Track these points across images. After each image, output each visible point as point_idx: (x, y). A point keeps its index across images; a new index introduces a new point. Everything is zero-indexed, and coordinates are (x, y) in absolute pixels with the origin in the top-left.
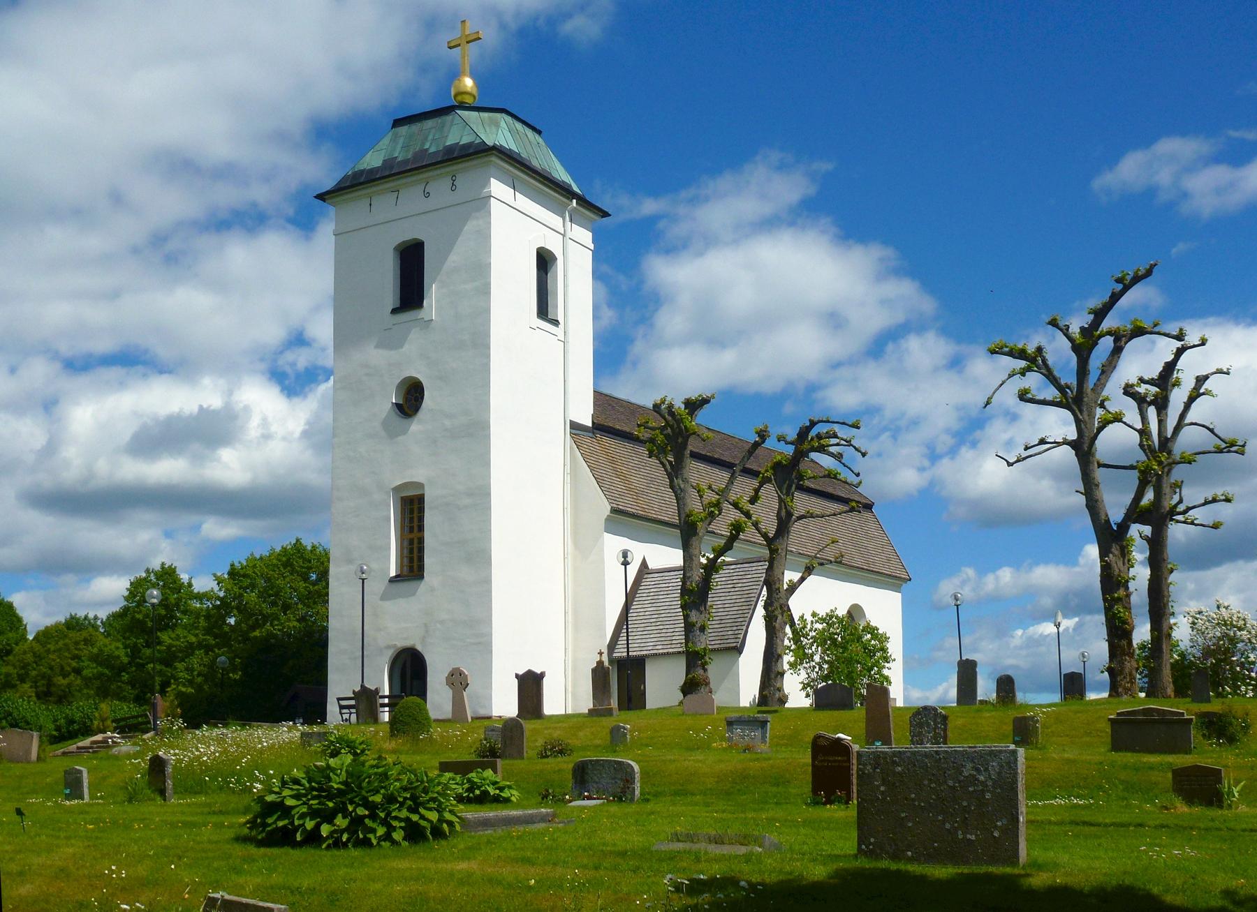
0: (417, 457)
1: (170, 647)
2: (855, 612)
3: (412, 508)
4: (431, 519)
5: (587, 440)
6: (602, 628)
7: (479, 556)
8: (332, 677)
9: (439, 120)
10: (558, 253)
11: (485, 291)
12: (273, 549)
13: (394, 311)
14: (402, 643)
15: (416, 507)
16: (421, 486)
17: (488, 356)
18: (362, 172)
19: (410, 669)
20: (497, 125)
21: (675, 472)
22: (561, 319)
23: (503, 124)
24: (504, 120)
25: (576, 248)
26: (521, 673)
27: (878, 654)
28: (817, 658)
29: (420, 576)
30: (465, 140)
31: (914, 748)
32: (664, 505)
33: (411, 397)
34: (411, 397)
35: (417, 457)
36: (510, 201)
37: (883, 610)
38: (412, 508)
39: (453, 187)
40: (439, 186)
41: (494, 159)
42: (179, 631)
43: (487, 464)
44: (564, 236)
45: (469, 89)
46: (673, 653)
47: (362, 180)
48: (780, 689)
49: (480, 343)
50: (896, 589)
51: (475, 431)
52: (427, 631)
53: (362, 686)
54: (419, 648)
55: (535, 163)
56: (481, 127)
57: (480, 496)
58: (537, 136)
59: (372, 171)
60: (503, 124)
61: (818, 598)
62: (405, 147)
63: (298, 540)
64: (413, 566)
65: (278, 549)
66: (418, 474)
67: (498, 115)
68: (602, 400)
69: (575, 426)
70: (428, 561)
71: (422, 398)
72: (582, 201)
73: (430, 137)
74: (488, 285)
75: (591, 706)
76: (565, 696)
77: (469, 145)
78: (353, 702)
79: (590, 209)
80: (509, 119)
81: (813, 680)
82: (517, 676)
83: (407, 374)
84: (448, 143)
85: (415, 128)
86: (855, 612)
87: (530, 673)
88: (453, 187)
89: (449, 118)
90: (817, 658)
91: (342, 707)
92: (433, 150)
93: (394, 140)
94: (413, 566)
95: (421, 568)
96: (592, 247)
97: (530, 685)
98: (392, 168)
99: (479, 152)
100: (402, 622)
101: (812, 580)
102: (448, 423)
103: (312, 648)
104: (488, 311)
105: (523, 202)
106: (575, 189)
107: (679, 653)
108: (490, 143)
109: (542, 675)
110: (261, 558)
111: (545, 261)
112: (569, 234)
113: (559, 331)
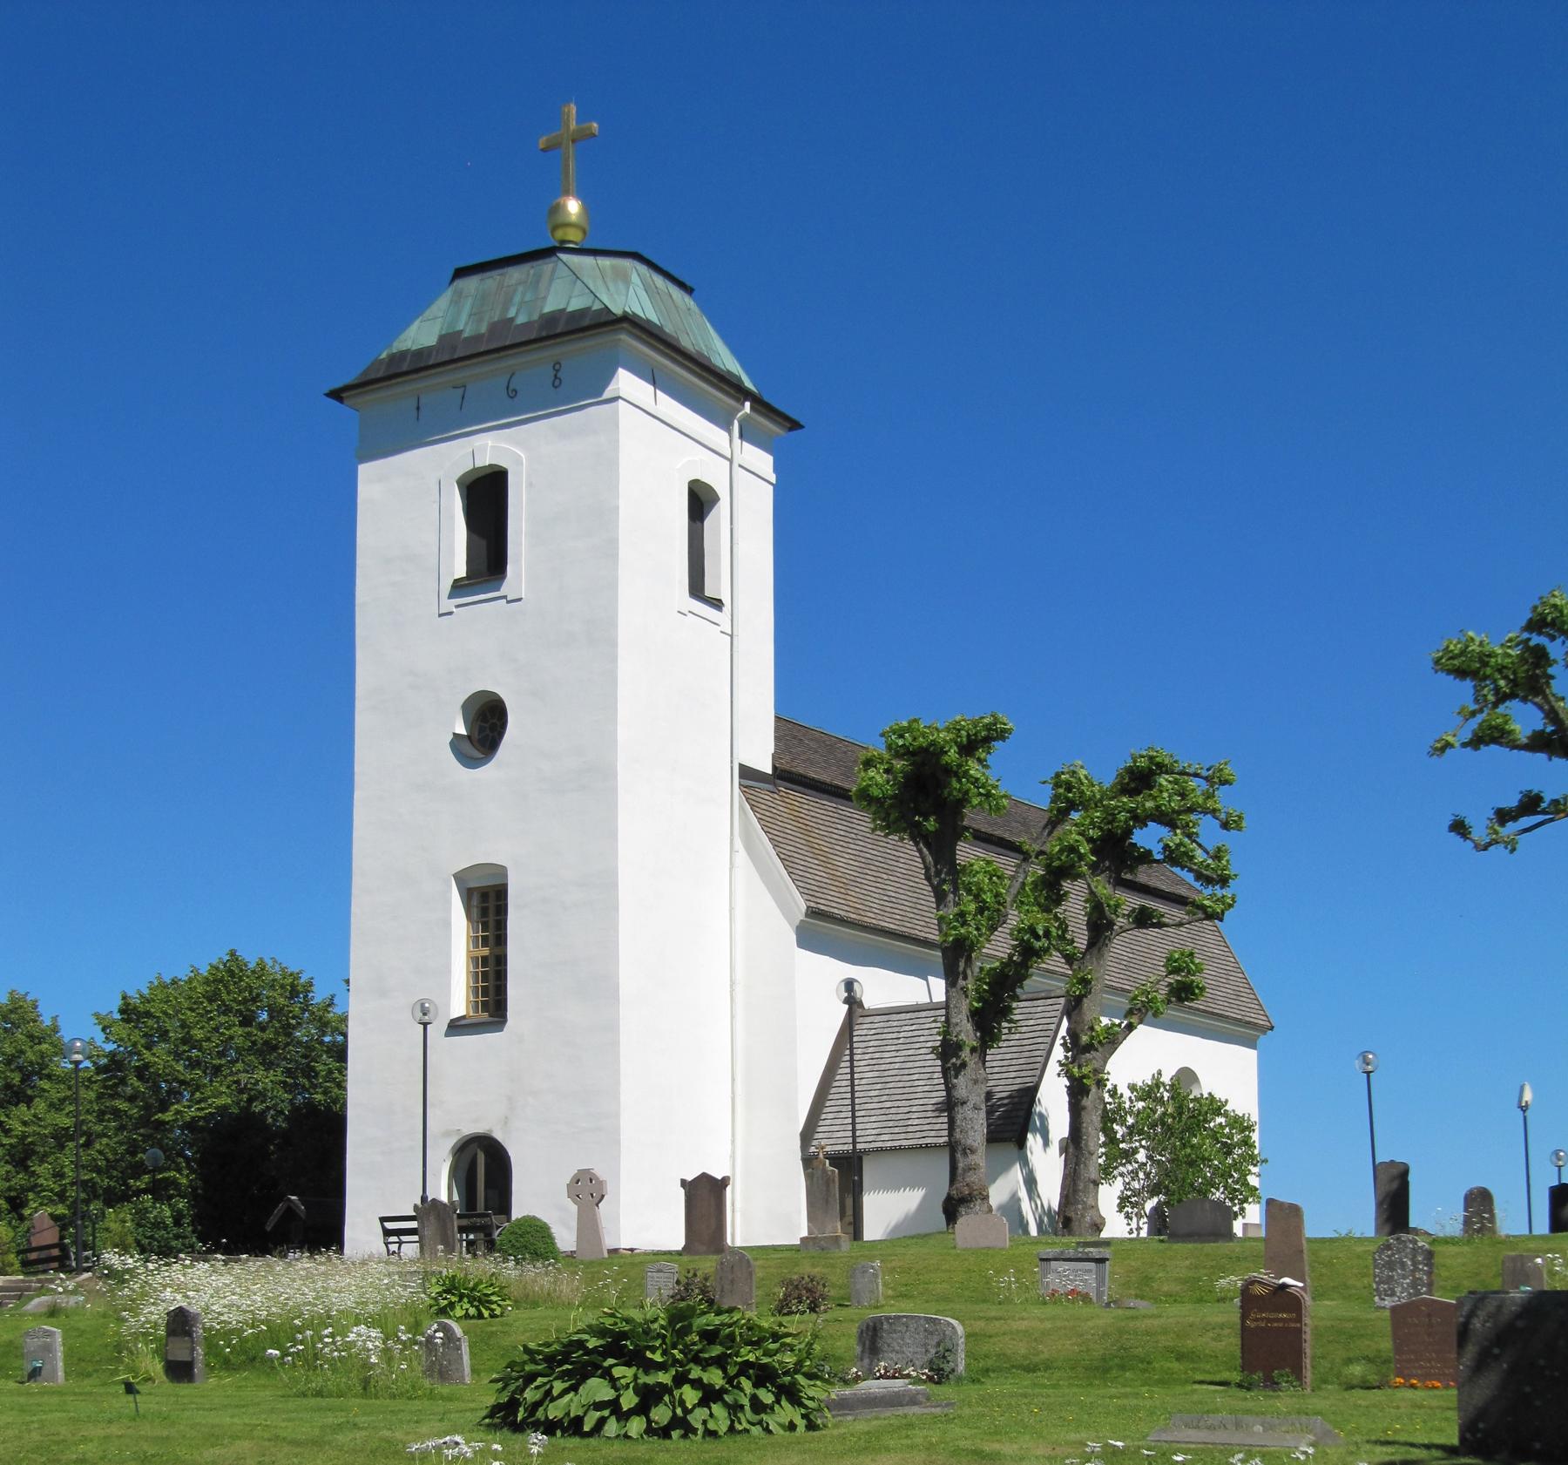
1: (24, 1137)
2: (1186, 1076)
7: (599, 986)
10: (722, 490)
11: (610, 551)
12: (195, 970)
14: (470, 1129)
15: (492, 904)
18: (403, 355)
19: (484, 1166)
21: (940, 849)
22: (726, 600)
23: (635, 278)
25: (749, 479)
26: (689, 1178)
27: (1238, 1151)
28: (1141, 1156)
30: (575, 305)
32: (918, 910)
33: (486, 725)
34: (486, 725)
37: (1229, 1075)
38: (488, 902)
42: (40, 1106)
43: (611, 834)
44: (731, 461)
45: (574, 218)
46: (911, 1148)
47: (405, 368)
48: (1095, 1207)
49: (599, 635)
50: (1251, 1044)
51: (592, 780)
53: (424, 1199)
54: (498, 1135)
55: (686, 343)
56: (600, 282)
57: (601, 888)
58: (687, 299)
59: (420, 353)
60: (635, 278)
61: (1143, 1058)
62: (476, 315)
63: (233, 953)
65: (204, 971)
67: (627, 263)
68: (786, 730)
69: (747, 773)
72: (759, 404)
73: (517, 299)
74: (613, 543)
75: (805, 1233)
76: (770, 1212)
77: (583, 313)
78: (414, 1225)
79: (772, 419)
80: (643, 269)
81: (1136, 1193)
82: (684, 1183)
84: (547, 310)
85: (491, 280)
86: (1186, 1076)
87: (704, 1178)
89: (546, 266)
90: (1141, 1156)
91: (388, 1233)
92: (521, 320)
93: (457, 300)
94: (492, 1000)
96: (773, 479)
97: (705, 1196)
98: (454, 348)
100: (477, 1087)
101: (1142, 1029)
103: (319, 1139)
104: (613, 585)
105: (668, 406)
106: (748, 384)
107: (936, 1146)
108: (617, 310)
110: (174, 982)
111: (700, 501)
113: (723, 617)
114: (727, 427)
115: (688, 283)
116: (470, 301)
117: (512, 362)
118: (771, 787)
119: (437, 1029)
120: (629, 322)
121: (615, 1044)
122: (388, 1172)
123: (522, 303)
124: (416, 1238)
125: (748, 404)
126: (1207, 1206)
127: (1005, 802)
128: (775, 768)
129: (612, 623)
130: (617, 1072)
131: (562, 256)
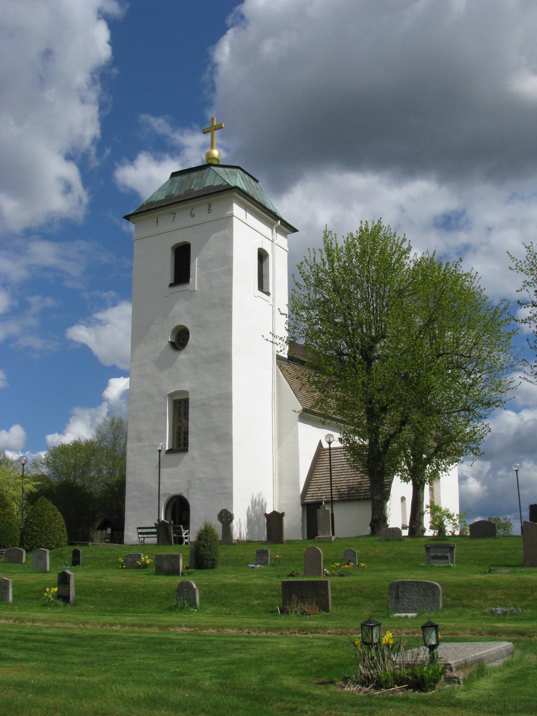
0: (185, 375)
3: (181, 407)
4: (192, 413)
5: (285, 365)
6: (297, 484)
7: (224, 437)
8: (128, 513)
9: (201, 172)
10: (268, 250)
11: (229, 272)
13: (171, 285)
16: (186, 393)
17: (231, 312)
19: (179, 508)
20: (236, 176)
23: (238, 175)
24: (239, 173)
29: (186, 450)
30: (217, 183)
31: (78, 547)
35: (185, 375)
36: (243, 219)
38: (181, 407)
39: (209, 211)
40: (201, 213)
41: (236, 194)
49: (226, 305)
51: (222, 359)
52: (190, 485)
53: (159, 520)
54: (185, 495)
55: (256, 199)
57: (226, 400)
58: (256, 183)
60: (238, 175)
64: (180, 443)
66: (185, 386)
70: (191, 440)
71: (187, 342)
73: (195, 182)
78: (155, 530)
80: (241, 172)
83: (179, 323)
84: (206, 186)
85: (185, 177)
87: (221, 513)
88: (209, 211)
89: (206, 171)
92: (196, 189)
94: (180, 443)
95: (186, 444)
96: (287, 250)
99: (227, 191)
102: (204, 353)
108: (233, 185)
109: (283, 515)
111: (262, 256)
112: (276, 241)
114: (272, 228)
115: (257, 179)
116: (177, 184)
117: (192, 204)
118: (287, 363)
119: (163, 453)
120: (236, 189)
121: (231, 460)
122: (141, 516)
123: (196, 184)
124: (156, 535)
125: (279, 221)
126: (409, 540)
127: (60, 684)
128: (288, 356)
129: (230, 299)
130: (232, 470)
131: (212, 168)
